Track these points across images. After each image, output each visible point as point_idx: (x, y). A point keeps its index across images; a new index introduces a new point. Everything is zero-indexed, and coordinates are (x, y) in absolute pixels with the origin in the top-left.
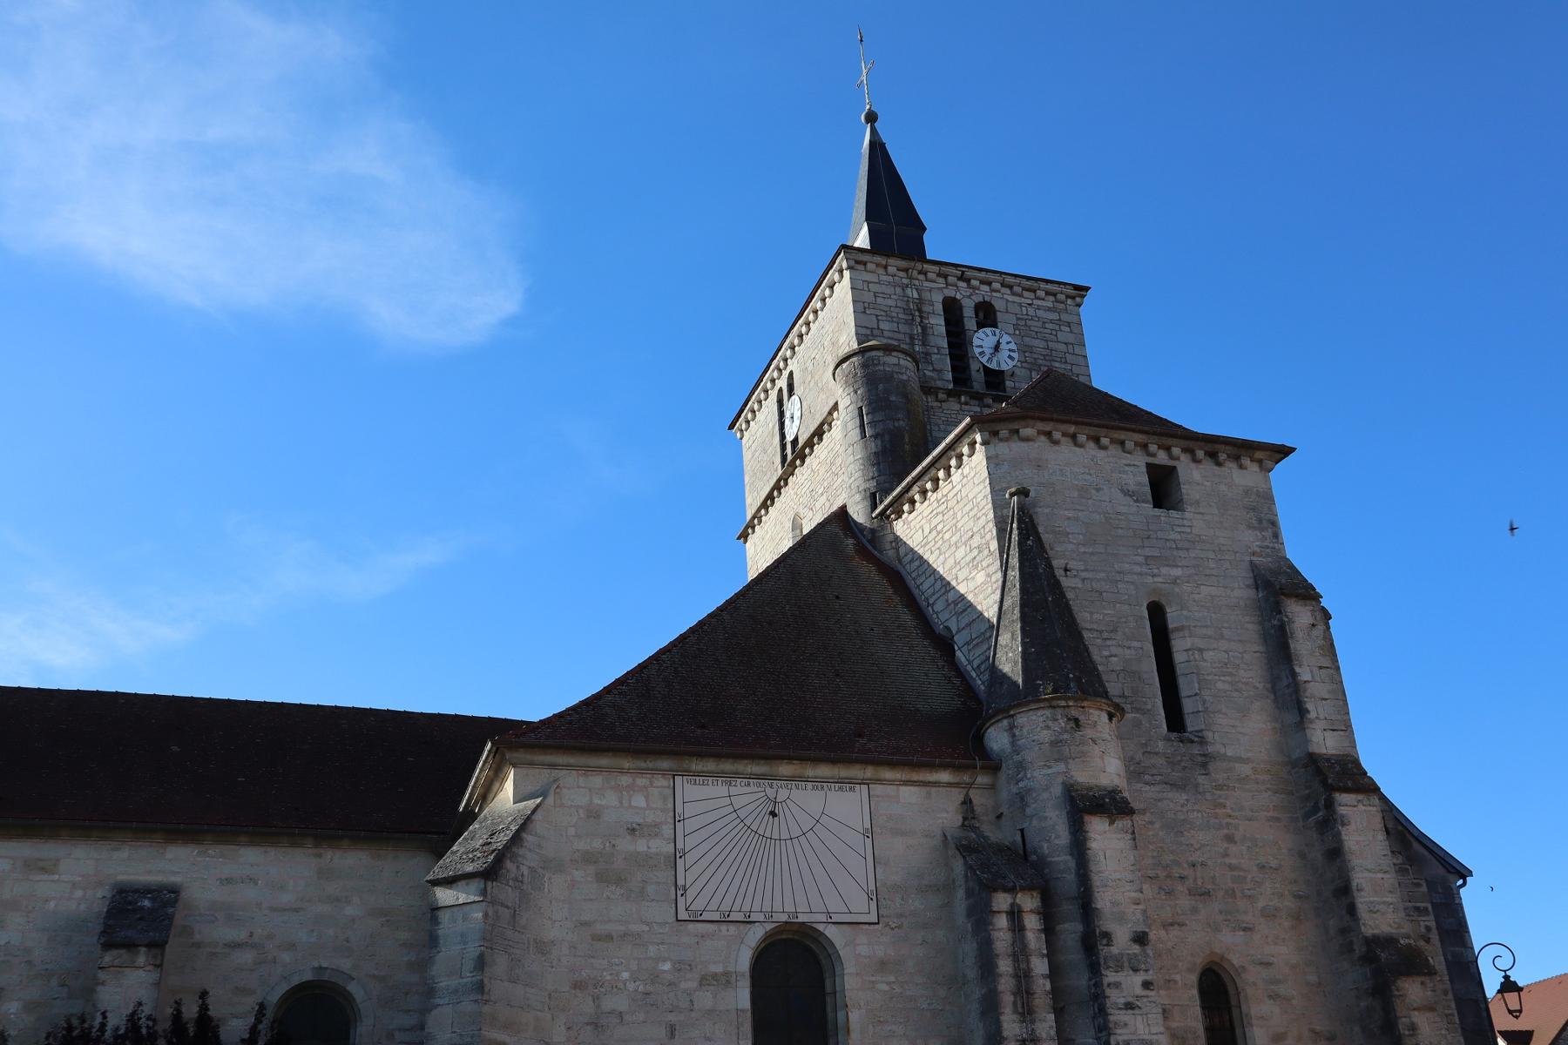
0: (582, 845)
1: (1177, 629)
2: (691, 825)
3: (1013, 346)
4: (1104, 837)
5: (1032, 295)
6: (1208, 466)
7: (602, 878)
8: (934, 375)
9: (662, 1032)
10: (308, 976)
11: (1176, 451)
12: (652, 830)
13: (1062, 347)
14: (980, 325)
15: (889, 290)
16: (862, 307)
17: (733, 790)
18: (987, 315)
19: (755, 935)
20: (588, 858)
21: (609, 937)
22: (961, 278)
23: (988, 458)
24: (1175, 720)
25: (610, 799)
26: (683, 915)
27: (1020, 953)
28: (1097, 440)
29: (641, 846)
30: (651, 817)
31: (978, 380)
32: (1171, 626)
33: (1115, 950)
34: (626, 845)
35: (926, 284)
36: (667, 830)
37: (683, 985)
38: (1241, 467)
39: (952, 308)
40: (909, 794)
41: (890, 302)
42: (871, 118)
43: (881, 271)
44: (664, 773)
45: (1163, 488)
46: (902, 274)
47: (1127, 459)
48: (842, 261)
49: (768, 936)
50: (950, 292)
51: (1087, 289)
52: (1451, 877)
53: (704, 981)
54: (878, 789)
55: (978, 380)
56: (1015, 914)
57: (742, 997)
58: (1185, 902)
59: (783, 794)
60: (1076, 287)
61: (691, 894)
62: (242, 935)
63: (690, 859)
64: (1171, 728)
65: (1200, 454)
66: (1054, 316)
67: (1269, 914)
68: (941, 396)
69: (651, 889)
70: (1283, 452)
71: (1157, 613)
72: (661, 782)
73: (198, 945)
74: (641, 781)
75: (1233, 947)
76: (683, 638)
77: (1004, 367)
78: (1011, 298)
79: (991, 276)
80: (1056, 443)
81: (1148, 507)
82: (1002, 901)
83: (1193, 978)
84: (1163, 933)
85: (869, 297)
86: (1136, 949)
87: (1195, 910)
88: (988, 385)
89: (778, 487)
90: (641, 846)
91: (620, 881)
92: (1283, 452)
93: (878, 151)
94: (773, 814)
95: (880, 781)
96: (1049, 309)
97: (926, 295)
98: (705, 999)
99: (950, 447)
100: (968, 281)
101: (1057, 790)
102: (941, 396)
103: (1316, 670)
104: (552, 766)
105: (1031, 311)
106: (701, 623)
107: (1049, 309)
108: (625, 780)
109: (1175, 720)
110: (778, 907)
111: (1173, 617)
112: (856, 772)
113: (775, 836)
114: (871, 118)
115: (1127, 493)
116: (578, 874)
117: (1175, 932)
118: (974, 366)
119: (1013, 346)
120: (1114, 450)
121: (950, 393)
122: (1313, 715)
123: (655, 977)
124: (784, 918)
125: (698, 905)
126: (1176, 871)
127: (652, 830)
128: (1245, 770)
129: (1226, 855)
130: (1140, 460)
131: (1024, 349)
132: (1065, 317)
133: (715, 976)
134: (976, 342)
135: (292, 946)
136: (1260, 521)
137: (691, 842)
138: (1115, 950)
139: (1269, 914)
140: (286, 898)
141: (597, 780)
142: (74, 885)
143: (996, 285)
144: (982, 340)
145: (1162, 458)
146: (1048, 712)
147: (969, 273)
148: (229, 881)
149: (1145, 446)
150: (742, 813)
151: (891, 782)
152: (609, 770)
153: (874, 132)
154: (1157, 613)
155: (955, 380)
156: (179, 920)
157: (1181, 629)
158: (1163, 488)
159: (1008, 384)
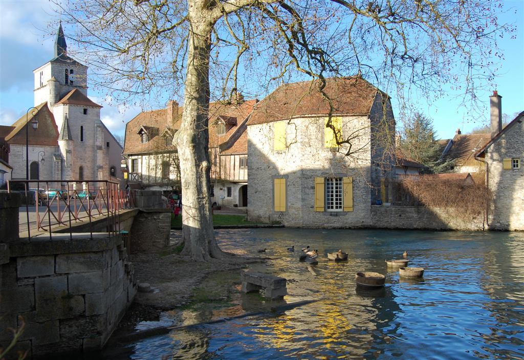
12: (20, 152)
14: (71, 73)
18: (72, 72)
24: (82, 140)
25: (16, 148)
27: (58, 166)
29: (19, 153)
31: (69, 82)
34: (17, 153)
39: (67, 70)
45: (85, 112)
50: (67, 68)
58: (79, 160)
67: (89, 161)
71: (82, 127)
75: (84, 165)
83: (79, 168)
90: (19, 153)
93: (61, 30)
109: (82, 140)
111: (84, 128)
113: (107, 213)
127: (20, 152)
139: (89, 161)
145: (86, 108)
153: (61, 25)
154: (82, 127)
158: (85, 112)
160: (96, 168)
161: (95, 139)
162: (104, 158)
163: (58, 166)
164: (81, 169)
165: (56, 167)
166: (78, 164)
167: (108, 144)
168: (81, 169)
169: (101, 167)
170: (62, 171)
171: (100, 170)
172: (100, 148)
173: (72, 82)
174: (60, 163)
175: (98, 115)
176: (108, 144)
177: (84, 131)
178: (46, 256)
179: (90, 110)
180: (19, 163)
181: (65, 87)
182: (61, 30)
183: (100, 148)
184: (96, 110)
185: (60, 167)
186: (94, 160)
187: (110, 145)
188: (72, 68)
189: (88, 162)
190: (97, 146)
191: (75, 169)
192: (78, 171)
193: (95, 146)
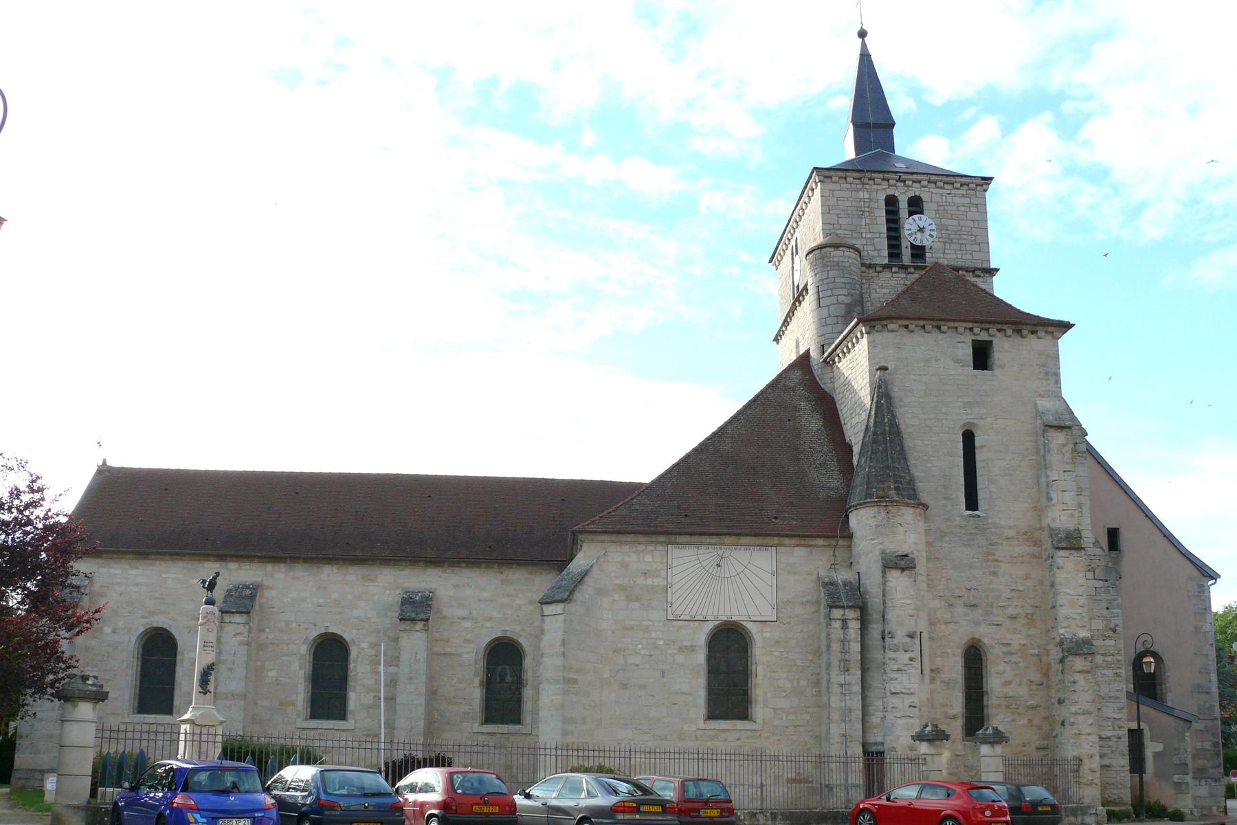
0: (618, 582)
1: (982, 447)
2: (676, 570)
3: (933, 227)
4: (897, 580)
5: (950, 187)
6: (1016, 340)
7: (629, 599)
8: (876, 254)
9: (658, 675)
10: (499, 634)
11: (992, 331)
13: (970, 224)
14: (911, 214)
15: (847, 194)
16: (827, 209)
17: (700, 551)
18: (916, 205)
19: (708, 627)
20: (622, 588)
21: (632, 628)
22: (899, 180)
23: (869, 343)
24: (972, 502)
25: (634, 557)
26: (670, 617)
27: (844, 642)
28: (939, 328)
29: (649, 582)
30: (655, 566)
31: (906, 254)
32: (977, 444)
33: (896, 641)
34: (641, 581)
35: (875, 187)
36: (663, 573)
37: (670, 651)
38: (1039, 338)
39: (891, 202)
40: (799, 552)
41: (849, 203)
42: (862, 34)
43: (843, 181)
44: (662, 543)
45: (982, 357)
46: (857, 181)
47: (962, 338)
48: (815, 177)
49: (716, 627)
50: (890, 192)
51: (987, 180)
52: (1205, 579)
53: (681, 649)
54: (781, 549)
55: (906, 254)
56: (844, 622)
57: (701, 658)
58: (960, 610)
59: (727, 553)
60: (984, 179)
61: (675, 606)
62: (465, 613)
63: (675, 588)
64: (490, 716)
65: (1009, 332)
66: (966, 201)
68: (879, 269)
69: (653, 604)
70: (1065, 326)
71: (969, 438)
72: (660, 548)
73: (444, 618)
74: (650, 548)
75: (988, 635)
76: (688, 456)
77: (925, 243)
78: (935, 191)
79: (919, 177)
80: (912, 332)
81: (970, 370)
82: (837, 613)
83: (959, 652)
84: (943, 627)
85: (833, 201)
86: (908, 640)
87: (966, 614)
88: (913, 256)
89: (786, 323)
90: (649, 582)
91: (637, 600)
92: (1065, 326)
93: (866, 61)
94: (719, 565)
95: (781, 545)
96: (963, 196)
97: (874, 195)
98: (680, 659)
99: (835, 350)
100: (904, 181)
101: (877, 552)
102: (879, 269)
103: (1062, 474)
104: (603, 542)
105: (949, 199)
106: (701, 444)
107: (963, 196)
108: (641, 548)
109: (972, 502)
110: (721, 612)
112: (768, 540)
114: (862, 34)
115: (956, 361)
116: (616, 597)
117: (952, 626)
118: (905, 244)
119: (933, 227)
120: (950, 333)
121: (884, 266)
122: (1055, 501)
123: (656, 647)
124: (725, 618)
125: (679, 612)
126: (958, 593)
127: (656, 574)
128: (1012, 533)
129: (991, 583)
130: (968, 338)
131: (941, 228)
132: (974, 201)
133: (686, 647)
134: (907, 226)
135: (490, 619)
136: (1047, 374)
137: (676, 579)
138: (896, 641)
140: (486, 595)
141: (626, 548)
142: (385, 588)
143: (925, 183)
144: (910, 226)
145: (984, 336)
146: (876, 509)
147: (904, 177)
148: (457, 586)
149: (971, 329)
150: (704, 564)
151: (789, 546)
152: (633, 543)
154: (969, 438)
155: (891, 255)
156: (435, 606)
157: (982, 447)
158: (982, 357)
159: (928, 255)
160: (1056, 653)
161: (1042, 497)
162: (1094, 598)
163: (844, 642)
164: (974, 658)
165: (836, 647)
166: (959, 636)
167: (1113, 537)
168: (974, 658)
169: (1081, 648)
170: (864, 669)
171: (1079, 663)
172: (1071, 542)
173: (918, 252)
174: (854, 625)
175: (1050, 372)
176: (1113, 537)
177: (980, 456)
178: (737, 535)
179: (1004, 348)
180: (647, 630)
181: (886, 274)
182: (866, 61)
183: (1071, 542)
184: (1035, 344)
185: (856, 647)
186: (1044, 610)
187: (1125, 539)
188: (915, 190)
189: (1008, 623)
190: (1053, 533)
191: (939, 662)
192: (955, 669)
193: (1046, 534)
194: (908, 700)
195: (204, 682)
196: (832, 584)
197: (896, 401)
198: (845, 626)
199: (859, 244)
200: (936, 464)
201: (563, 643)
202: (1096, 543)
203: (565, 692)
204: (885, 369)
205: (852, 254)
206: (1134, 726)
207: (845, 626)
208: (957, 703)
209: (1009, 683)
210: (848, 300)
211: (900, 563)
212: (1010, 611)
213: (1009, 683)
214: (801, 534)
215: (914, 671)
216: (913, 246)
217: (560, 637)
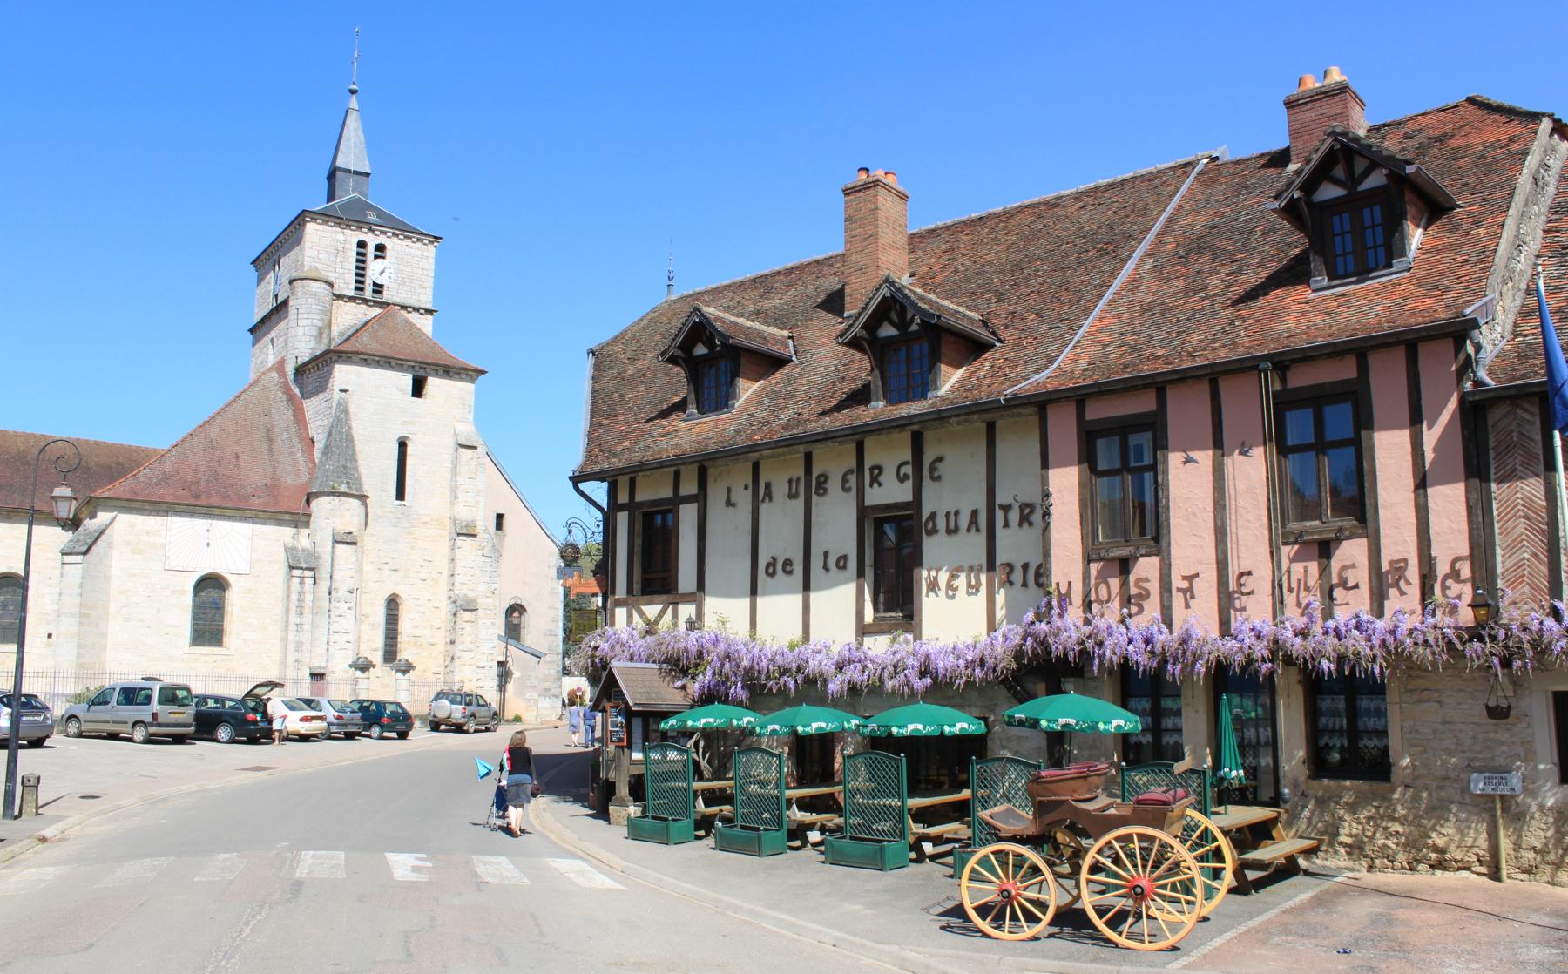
14: (376, 257)
24: (401, 495)
31: (369, 288)
39: (362, 244)
45: (418, 389)
55: (369, 288)
70: (482, 372)
71: (403, 445)
109: (401, 495)
144: (374, 269)
155: (357, 288)
158: (418, 389)
171: (467, 615)
173: (378, 288)
194: (346, 637)
195: (932, 469)
196: (294, 549)
197: (352, 416)
198: (302, 582)
199: (332, 277)
200: (376, 469)
201: (81, 586)
202: (486, 530)
203: (81, 624)
204: (345, 391)
205: (324, 286)
206: (502, 659)
207: (302, 582)
208: (379, 640)
209: (416, 627)
210: (320, 324)
211: (347, 540)
212: (421, 575)
213: (416, 627)
214: (275, 516)
215: (351, 617)
216: (375, 284)
217: (79, 580)
